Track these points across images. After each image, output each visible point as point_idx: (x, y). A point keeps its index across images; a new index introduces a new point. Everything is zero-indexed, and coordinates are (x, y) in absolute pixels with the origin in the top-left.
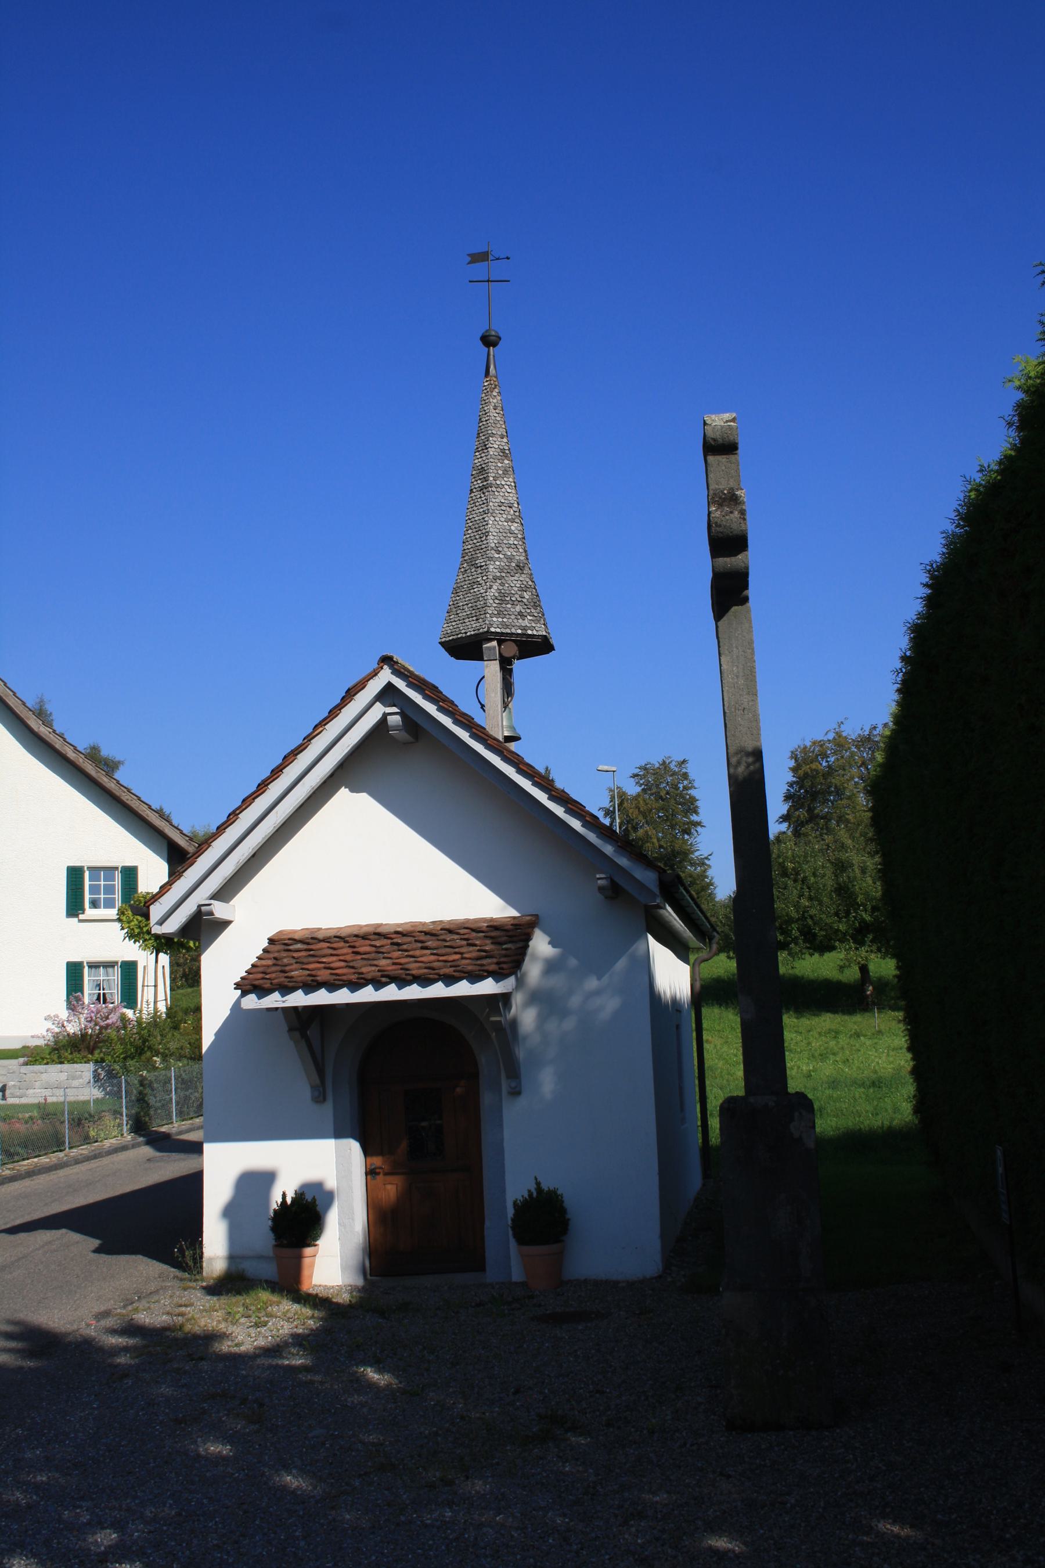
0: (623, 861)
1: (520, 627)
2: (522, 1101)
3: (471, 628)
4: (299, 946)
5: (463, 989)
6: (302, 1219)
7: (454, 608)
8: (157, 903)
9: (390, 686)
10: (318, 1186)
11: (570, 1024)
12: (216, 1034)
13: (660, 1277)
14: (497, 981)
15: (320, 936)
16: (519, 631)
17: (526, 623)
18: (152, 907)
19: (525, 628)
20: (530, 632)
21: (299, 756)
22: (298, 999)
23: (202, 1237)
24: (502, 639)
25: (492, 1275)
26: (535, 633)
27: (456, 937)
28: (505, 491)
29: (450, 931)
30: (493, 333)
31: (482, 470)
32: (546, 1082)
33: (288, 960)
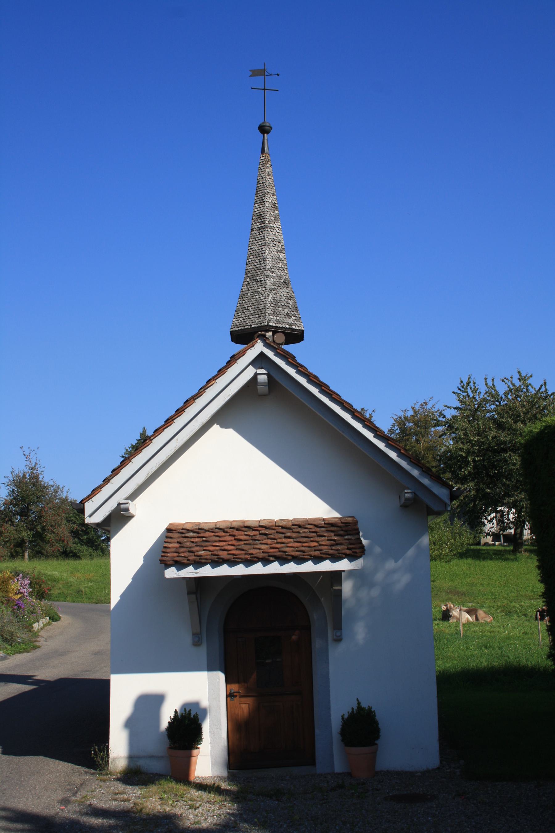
0: (426, 481)
1: (288, 324)
2: (342, 647)
3: (254, 322)
4: (191, 534)
5: (308, 567)
6: (187, 728)
7: (241, 309)
8: (90, 501)
9: (262, 355)
10: (196, 704)
11: (375, 592)
12: (121, 596)
13: (438, 768)
14: (351, 561)
15: (206, 528)
16: (287, 326)
17: (291, 321)
18: (86, 504)
19: (290, 325)
20: (294, 327)
21: (196, 401)
22: (189, 572)
23: (108, 743)
24: (275, 330)
25: (320, 768)
26: (297, 328)
27: (306, 530)
28: (276, 232)
29: (300, 526)
30: (268, 125)
31: (260, 216)
32: (359, 632)
33: (180, 544)
